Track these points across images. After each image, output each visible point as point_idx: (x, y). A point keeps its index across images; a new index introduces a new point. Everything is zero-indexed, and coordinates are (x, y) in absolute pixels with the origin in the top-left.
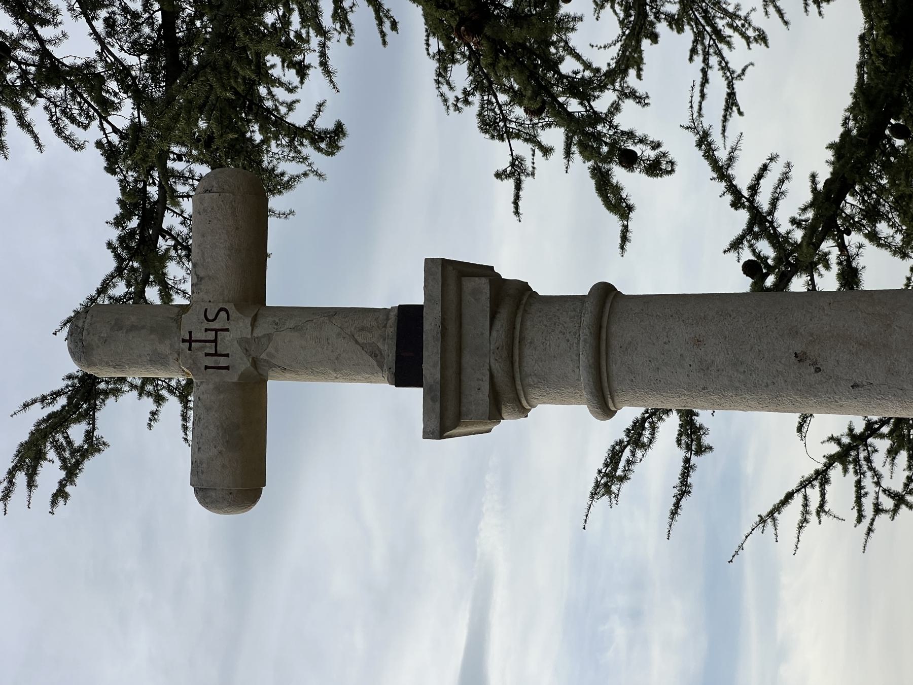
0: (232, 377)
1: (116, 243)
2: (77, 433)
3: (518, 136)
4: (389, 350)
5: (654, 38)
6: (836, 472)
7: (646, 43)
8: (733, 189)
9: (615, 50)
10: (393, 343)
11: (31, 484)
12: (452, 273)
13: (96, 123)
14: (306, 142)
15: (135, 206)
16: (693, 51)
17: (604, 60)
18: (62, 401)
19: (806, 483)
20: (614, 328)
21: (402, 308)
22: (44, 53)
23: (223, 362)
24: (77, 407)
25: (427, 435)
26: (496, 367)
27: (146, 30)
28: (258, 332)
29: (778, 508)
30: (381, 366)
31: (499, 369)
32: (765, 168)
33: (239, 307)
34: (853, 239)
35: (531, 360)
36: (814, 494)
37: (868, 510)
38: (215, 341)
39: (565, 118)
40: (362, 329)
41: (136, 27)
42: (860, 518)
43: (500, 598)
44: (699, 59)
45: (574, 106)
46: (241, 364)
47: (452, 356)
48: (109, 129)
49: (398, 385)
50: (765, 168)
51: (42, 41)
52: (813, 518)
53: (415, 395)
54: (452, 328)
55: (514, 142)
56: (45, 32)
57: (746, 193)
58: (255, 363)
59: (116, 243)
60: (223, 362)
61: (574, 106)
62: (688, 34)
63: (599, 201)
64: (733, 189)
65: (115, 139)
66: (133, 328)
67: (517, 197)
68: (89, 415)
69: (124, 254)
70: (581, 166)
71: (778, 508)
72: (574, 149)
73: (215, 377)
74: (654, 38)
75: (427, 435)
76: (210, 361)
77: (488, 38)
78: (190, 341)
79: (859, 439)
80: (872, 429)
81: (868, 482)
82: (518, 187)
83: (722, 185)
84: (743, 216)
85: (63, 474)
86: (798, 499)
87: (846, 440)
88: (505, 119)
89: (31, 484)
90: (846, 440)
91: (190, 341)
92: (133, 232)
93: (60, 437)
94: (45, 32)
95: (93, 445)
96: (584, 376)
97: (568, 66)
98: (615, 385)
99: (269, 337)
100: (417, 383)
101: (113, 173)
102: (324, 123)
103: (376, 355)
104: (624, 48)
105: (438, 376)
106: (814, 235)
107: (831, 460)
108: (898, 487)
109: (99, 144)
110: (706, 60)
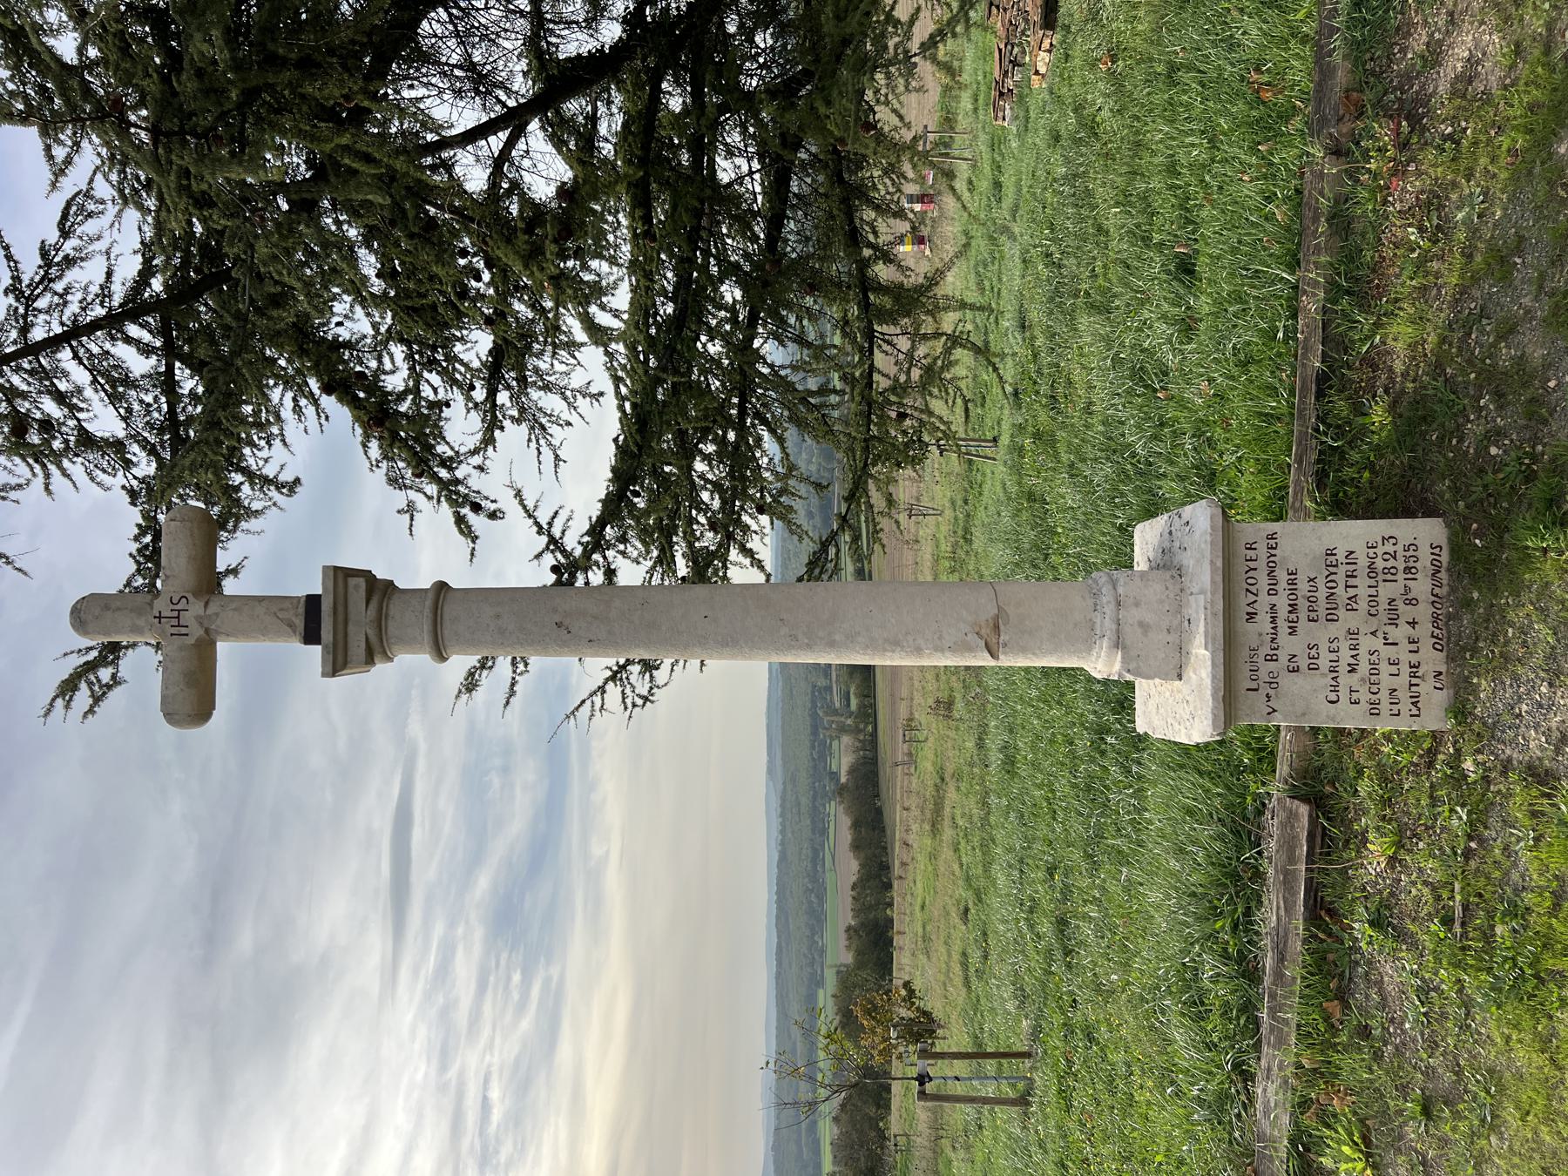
0: (191, 640)
1: (135, 553)
2: (105, 674)
3: (411, 488)
4: (300, 623)
5: (502, 428)
6: (610, 685)
7: (497, 433)
8: (537, 524)
9: (479, 436)
10: (303, 618)
11: (67, 706)
12: (341, 576)
13: (120, 473)
14: (272, 488)
15: (148, 527)
16: (529, 440)
17: (473, 441)
18: (94, 654)
19: (594, 693)
20: (445, 608)
21: (308, 597)
22: (81, 429)
23: (183, 631)
24: (106, 657)
25: (324, 675)
26: (369, 631)
27: (156, 415)
28: (209, 612)
29: (577, 709)
30: (294, 632)
31: (372, 633)
32: (556, 513)
33: (195, 595)
34: (610, 554)
35: (393, 628)
36: (597, 700)
37: (630, 706)
38: (178, 617)
39: (436, 479)
40: (282, 610)
41: (148, 413)
42: (626, 708)
43: (421, 764)
44: (533, 445)
45: (443, 473)
46: (196, 632)
47: (341, 627)
48: (130, 477)
49: (306, 643)
50: (556, 513)
51: (78, 420)
52: (597, 713)
53: (317, 649)
54: (340, 609)
55: (409, 491)
56: (81, 415)
57: (545, 527)
58: (207, 631)
59: (135, 553)
60: (183, 631)
61: (443, 473)
62: (524, 428)
63: (455, 529)
64: (537, 524)
65: (135, 483)
66: (118, 609)
67: (411, 525)
68: (115, 663)
69: (141, 560)
70: (446, 510)
71: (577, 709)
72: (443, 499)
73: (178, 641)
74: (502, 428)
75: (324, 675)
76: (174, 630)
77: (388, 429)
78: (160, 617)
79: (623, 668)
80: (629, 662)
81: (628, 691)
82: (412, 519)
83: (531, 521)
84: (544, 539)
85: (90, 701)
86: (588, 703)
87: (615, 668)
88: (403, 478)
89: (67, 706)
90: (615, 668)
91: (160, 617)
92: (146, 546)
93: (92, 678)
94: (81, 415)
95: (116, 681)
96: (427, 637)
97: (442, 448)
98: (446, 643)
99: (217, 615)
100: (319, 643)
101: (135, 505)
102: (286, 477)
103: (291, 625)
104: (485, 434)
105: (331, 639)
106: (587, 554)
107: (607, 681)
108: (645, 693)
109: (124, 487)
110: (538, 441)
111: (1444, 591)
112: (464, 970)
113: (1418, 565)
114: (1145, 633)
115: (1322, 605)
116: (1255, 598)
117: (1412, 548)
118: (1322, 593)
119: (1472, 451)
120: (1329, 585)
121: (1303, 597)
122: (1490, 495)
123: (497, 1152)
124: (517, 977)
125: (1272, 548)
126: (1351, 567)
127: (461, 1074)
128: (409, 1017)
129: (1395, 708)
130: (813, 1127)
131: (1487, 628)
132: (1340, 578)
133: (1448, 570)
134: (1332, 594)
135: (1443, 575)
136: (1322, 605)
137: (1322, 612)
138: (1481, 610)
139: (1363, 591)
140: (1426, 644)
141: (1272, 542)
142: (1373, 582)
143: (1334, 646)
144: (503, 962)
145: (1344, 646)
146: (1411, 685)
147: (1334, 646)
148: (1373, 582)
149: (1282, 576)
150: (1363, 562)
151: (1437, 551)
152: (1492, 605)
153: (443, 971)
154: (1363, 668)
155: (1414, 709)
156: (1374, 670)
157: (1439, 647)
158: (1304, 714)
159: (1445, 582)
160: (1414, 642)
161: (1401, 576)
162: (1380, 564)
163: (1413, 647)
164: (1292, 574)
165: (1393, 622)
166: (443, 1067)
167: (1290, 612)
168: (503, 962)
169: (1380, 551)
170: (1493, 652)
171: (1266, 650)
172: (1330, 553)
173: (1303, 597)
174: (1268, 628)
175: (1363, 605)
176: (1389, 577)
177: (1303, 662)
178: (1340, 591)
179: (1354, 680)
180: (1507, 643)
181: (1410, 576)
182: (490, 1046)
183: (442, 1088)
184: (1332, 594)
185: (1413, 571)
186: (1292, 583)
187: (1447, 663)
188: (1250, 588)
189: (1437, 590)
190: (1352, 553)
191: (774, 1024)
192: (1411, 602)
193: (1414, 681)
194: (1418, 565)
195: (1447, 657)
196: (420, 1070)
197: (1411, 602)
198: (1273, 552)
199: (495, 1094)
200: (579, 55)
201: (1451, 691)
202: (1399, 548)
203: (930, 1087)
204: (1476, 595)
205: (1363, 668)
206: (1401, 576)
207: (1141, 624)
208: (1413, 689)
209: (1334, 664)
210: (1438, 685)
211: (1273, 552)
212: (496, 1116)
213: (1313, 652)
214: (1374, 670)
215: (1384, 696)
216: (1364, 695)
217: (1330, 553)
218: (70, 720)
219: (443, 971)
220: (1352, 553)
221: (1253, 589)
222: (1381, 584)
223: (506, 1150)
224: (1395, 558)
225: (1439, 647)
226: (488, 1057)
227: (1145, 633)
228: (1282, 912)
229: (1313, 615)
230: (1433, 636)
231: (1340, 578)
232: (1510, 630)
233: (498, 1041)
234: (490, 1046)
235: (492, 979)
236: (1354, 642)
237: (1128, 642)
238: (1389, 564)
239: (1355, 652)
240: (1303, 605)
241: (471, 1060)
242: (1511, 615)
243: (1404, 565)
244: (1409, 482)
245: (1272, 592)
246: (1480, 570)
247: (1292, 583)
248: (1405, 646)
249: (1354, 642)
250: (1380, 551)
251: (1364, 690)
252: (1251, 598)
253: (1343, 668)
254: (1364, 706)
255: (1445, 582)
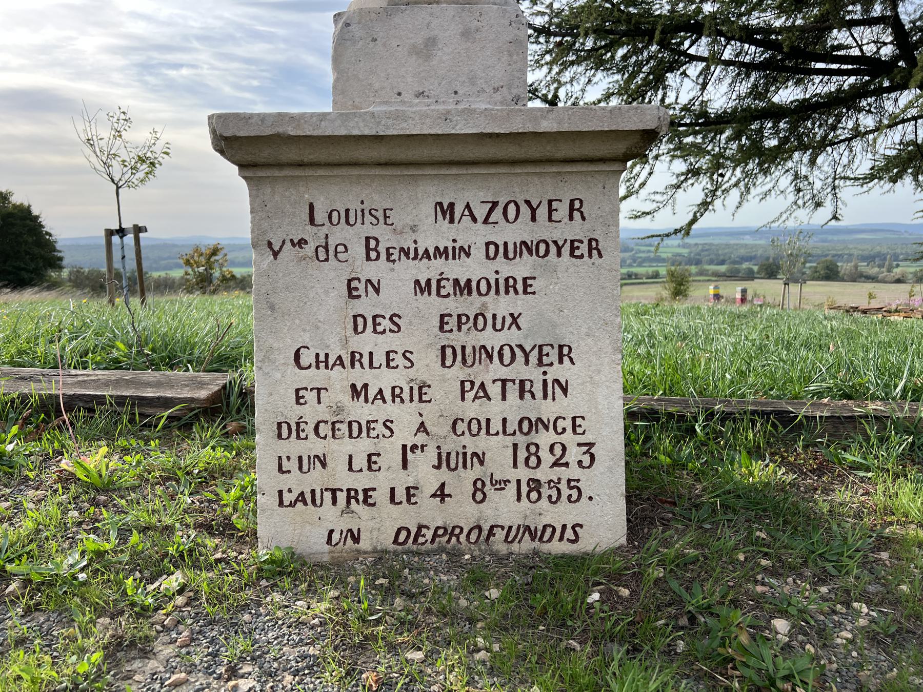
111: (498, 543)
112: (258, 49)
113: (544, 502)
114: (415, 51)
115: (470, 339)
116: (480, 219)
117: (574, 493)
118: (492, 339)
119: (759, 589)
120: (507, 352)
121: (484, 305)
122: (692, 619)
123: (151, 74)
124: (255, 83)
125: (573, 249)
126: (538, 389)
127: (196, 50)
128: (227, 15)
129: (293, 465)
130: (178, 266)
131: (429, 611)
132: (518, 370)
133: (536, 553)
134: (490, 357)
135: (526, 545)
136: (470, 339)
137: (457, 339)
138: (463, 603)
139: (495, 409)
140: (407, 517)
141: (584, 249)
142: (512, 426)
143: (399, 360)
144: (264, 74)
145: (398, 378)
146: (334, 491)
147: (399, 360)
148: (512, 426)
149: (521, 268)
150: (548, 410)
151: (569, 534)
152: (472, 621)
153: (257, 36)
154: (361, 411)
155: (292, 497)
156: (356, 429)
157: (402, 538)
158: (272, 308)
159: (515, 547)
160: (409, 496)
161: (524, 474)
162: (545, 438)
163: (401, 495)
164: (526, 286)
165: (443, 461)
166: (199, 38)
167: (456, 282)
168: (264, 74)
169: (568, 438)
170: (378, 622)
171: (386, 238)
172: (564, 353)
173: (484, 305)
174: (427, 242)
175: (472, 409)
176: (522, 454)
177: (367, 306)
178: (496, 370)
179: (339, 394)
180: (392, 648)
181: (524, 489)
182: (213, 68)
183: (186, 38)
184: (490, 357)
185: (534, 495)
186: (509, 286)
187: (375, 551)
188: (499, 210)
189: (500, 534)
190: (565, 391)
191: (237, 242)
192: (479, 491)
193: (342, 497)
194: (544, 502)
195: (385, 551)
196: (196, 23)
197: (479, 491)
198: (566, 250)
199: (184, 71)
200: (831, 93)
201: (326, 559)
202: (574, 472)
203: (116, 239)
204: (494, 593)
205: (361, 411)
206: (524, 474)
207: (431, 42)
208: (328, 496)
209: (366, 361)
210: (336, 537)
211: (566, 250)
212: (172, 73)
213: (385, 324)
214: (356, 429)
215: (314, 446)
216: (311, 412)
217: (564, 353)
218: (473, 404)
219: (257, 36)
220: (565, 391)
221: (497, 215)
222: (509, 441)
223: (150, 79)
224: (556, 464)
225: (402, 538)
226: (206, 66)
227: (415, 51)
228: (80, 378)
229: (452, 322)
230: (420, 527)
231: (518, 370)
232: (419, 655)
233: (217, 72)
234: (213, 68)
235: (253, 67)
236: (406, 396)
237: (397, 19)
238: (544, 454)
239: (388, 395)
240: (470, 305)
241: (204, 56)
242: (450, 655)
243: (543, 479)
244: (675, 504)
245: (493, 250)
246: (541, 600)
247: (509, 286)
248: (402, 481)
249: (406, 396)
250: (568, 438)
251: (322, 412)
252: (480, 212)
253: (359, 376)
254: (293, 413)
255: (515, 547)
